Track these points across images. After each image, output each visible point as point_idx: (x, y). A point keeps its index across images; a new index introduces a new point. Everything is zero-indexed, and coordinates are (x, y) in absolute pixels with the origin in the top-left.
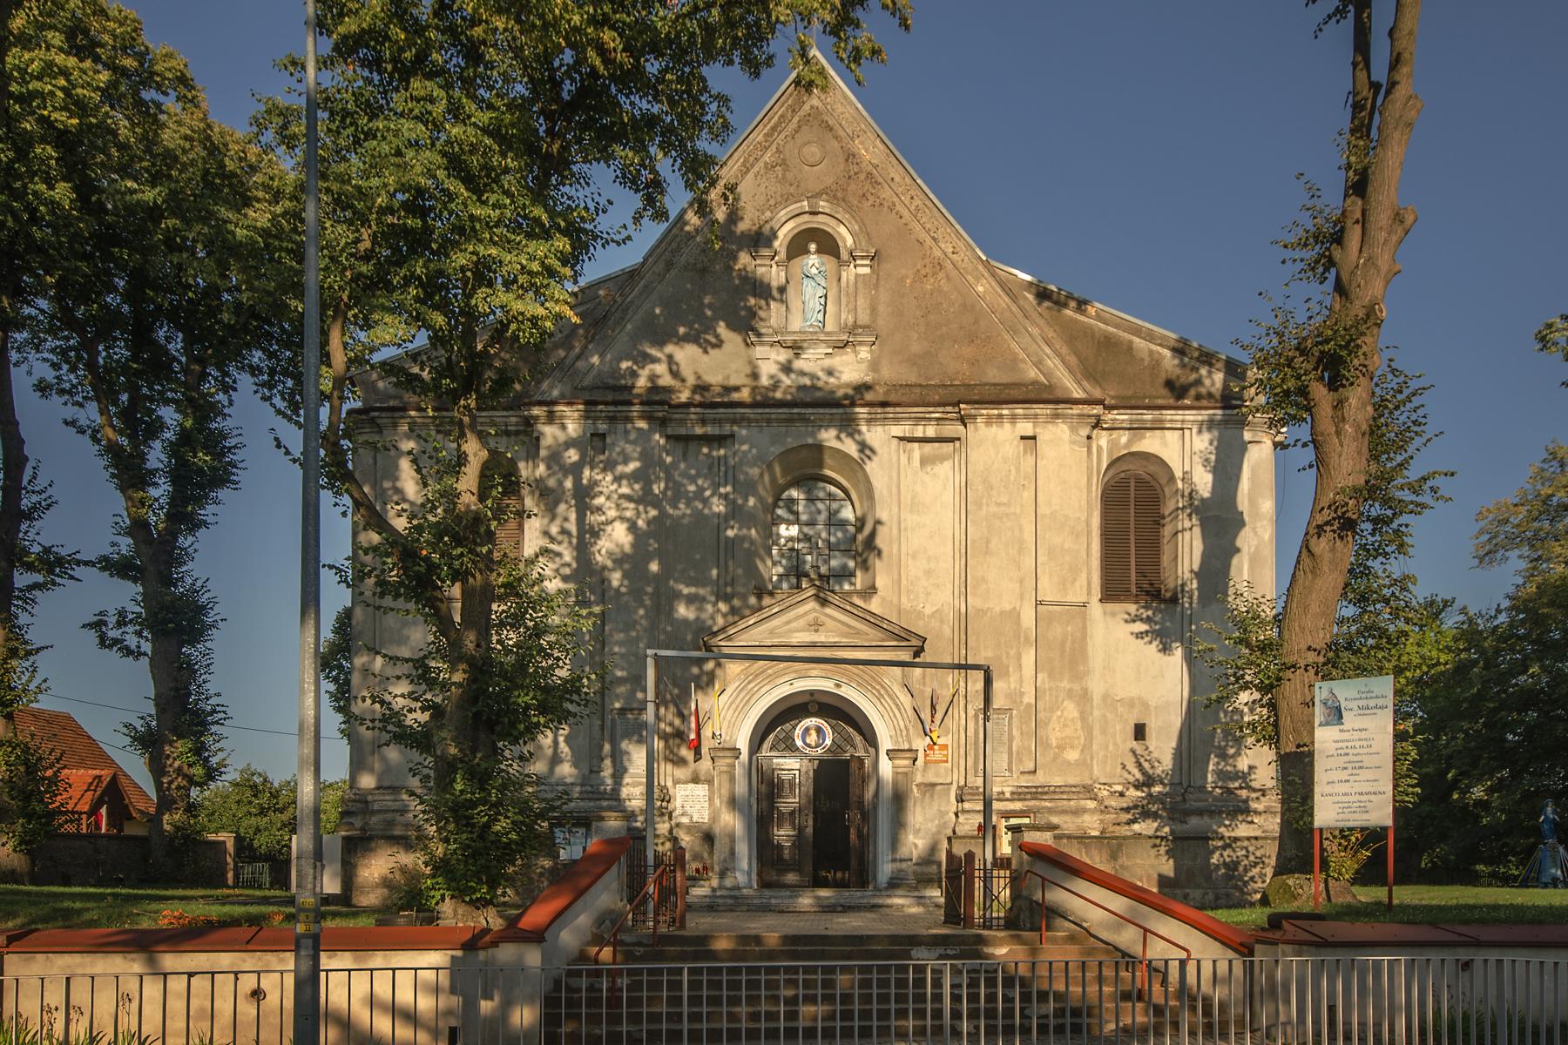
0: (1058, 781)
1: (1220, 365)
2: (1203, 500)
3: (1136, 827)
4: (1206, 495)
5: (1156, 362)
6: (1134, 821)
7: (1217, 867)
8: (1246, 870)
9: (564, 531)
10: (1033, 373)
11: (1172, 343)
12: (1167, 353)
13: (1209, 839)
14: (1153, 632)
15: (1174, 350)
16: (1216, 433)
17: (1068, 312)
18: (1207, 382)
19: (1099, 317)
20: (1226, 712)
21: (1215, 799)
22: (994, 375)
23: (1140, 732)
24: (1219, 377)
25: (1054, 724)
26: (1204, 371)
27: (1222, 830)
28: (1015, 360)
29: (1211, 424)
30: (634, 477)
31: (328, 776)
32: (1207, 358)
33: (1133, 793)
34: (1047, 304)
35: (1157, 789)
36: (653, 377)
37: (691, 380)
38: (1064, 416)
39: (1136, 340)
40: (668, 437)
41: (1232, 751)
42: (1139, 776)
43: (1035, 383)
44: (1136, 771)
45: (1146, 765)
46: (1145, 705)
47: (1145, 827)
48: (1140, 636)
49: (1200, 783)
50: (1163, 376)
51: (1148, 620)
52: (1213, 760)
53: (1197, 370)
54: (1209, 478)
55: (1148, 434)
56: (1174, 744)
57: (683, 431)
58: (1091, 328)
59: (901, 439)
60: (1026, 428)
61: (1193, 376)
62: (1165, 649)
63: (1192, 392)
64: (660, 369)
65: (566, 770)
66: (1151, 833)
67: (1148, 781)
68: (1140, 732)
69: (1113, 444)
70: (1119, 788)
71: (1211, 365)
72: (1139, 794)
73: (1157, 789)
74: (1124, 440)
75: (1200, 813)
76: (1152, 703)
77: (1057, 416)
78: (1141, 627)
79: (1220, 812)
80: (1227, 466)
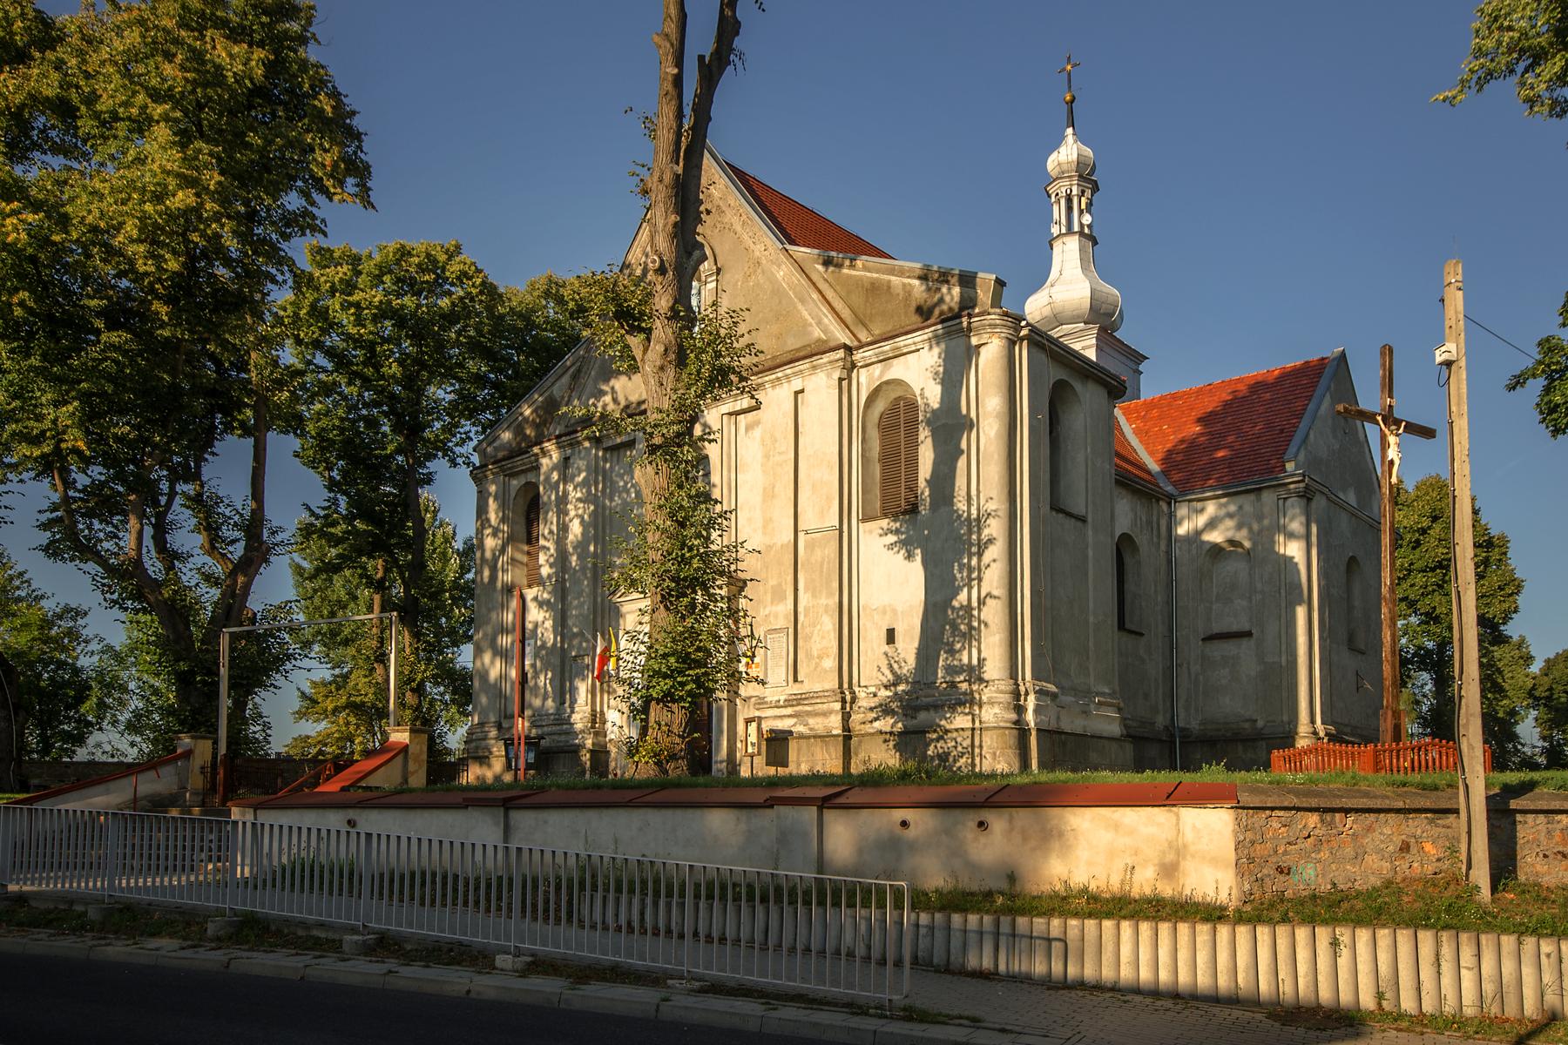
0: (818, 687)
1: (954, 280)
2: (934, 411)
3: (877, 724)
4: (936, 406)
5: (908, 290)
6: (876, 719)
7: (932, 758)
8: (955, 761)
9: (551, 532)
10: (817, 333)
11: (918, 272)
12: (917, 282)
13: (925, 732)
14: (900, 541)
15: (920, 278)
16: (943, 346)
17: (845, 271)
18: (947, 298)
19: (865, 268)
20: (953, 608)
21: (941, 694)
22: (792, 343)
23: (891, 636)
24: (956, 290)
25: (815, 638)
26: (944, 290)
27: (943, 722)
28: (806, 325)
29: (937, 339)
30: (585, 483)
31: (1213, 878)
32: (944, 277)
33: (884, 693)
34: (831, 269)
35: (901, 688)
36: (605, 406)
37: (623, 403)
38: (820, 366)
39: (893, 278)
40: (606, 450)
41: (958, 646)
42: (890, 677)
43: (819, 340)
44: (887, 672)
45: (895, 666)
46: (894, 611)
47: (885, 724)
48: (890, 547)
49: (931, 679)
50: (914, 305)
51: (897, 532)
52: (943, 656)
53: (939, 289)
54: (938, 388)
55: (895, 361)
56: (916, 644)
57: (610, 443)
58: (860, 278)
59: (730, 414)
60: (797, 384)
61: (937, 296)
62: (909, 556)
63: (937, 312)
64: (608, 399)
65: (550, 703)
66: (888, 729)
67: (898, 680)
68: (891, 636)
69: (870, 377)
70: (873, 689)
71: (947, 282)
72: (889, 693)
73: (901, 688)
74: (877, 372)
75: (927, 708)
76: (900, 609)
77: (814, 368)
78: (892, 538)
79: (942, 706)
80: (953, 376)
